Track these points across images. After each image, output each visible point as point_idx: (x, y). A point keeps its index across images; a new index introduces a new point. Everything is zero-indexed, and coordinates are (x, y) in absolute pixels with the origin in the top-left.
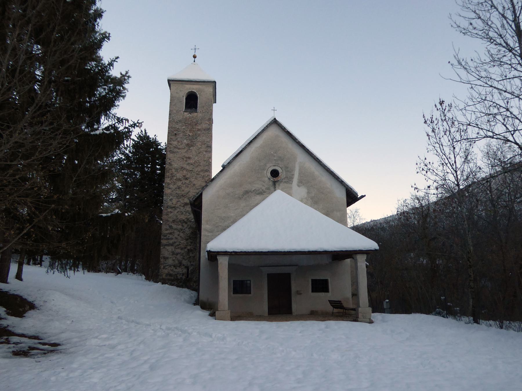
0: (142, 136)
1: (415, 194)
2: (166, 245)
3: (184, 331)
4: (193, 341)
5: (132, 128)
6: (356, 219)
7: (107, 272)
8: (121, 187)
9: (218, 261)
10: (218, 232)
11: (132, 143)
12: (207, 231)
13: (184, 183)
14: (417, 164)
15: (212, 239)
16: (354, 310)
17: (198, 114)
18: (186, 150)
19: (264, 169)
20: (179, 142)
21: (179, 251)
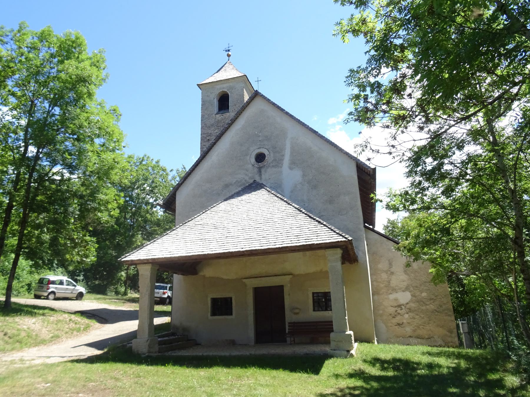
19: (247, 155)
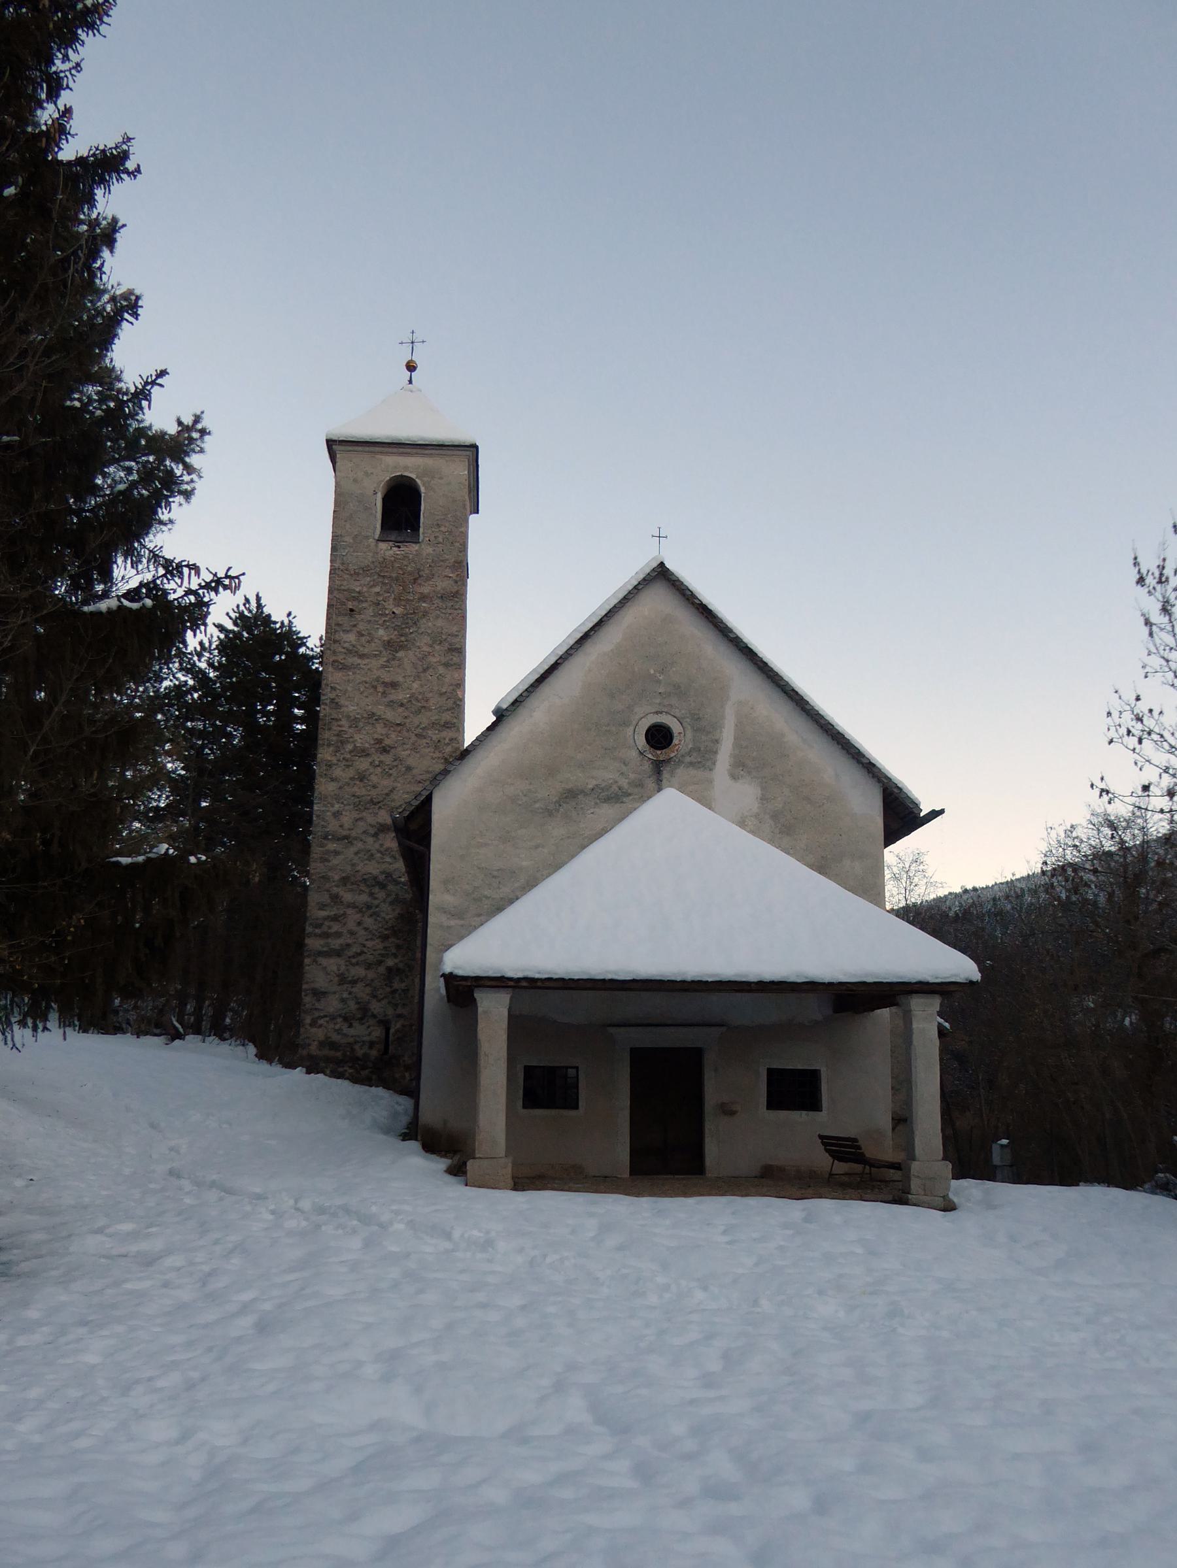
0: (249, 615)
1: (1102, 810)
2: (320, 954)
3: (366, 1220)
4: (394, 1249)
5: (208, 592)
6: (916, 885)
7: (139, 1033)
8: (183, 772)
9: (479, 1005)
10: (479, 915)
11: (218, 637)
12: (445, 912)
13: (377, 763)
14: (1109, 714)
15: (461, 938)
16: (896, 1166)
17: (423, 546)
18: (385, 659)
19: (625, 724)
20: (360, 634)
21: (360, 972)
